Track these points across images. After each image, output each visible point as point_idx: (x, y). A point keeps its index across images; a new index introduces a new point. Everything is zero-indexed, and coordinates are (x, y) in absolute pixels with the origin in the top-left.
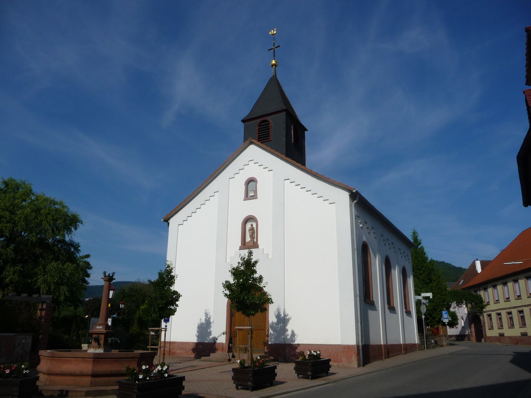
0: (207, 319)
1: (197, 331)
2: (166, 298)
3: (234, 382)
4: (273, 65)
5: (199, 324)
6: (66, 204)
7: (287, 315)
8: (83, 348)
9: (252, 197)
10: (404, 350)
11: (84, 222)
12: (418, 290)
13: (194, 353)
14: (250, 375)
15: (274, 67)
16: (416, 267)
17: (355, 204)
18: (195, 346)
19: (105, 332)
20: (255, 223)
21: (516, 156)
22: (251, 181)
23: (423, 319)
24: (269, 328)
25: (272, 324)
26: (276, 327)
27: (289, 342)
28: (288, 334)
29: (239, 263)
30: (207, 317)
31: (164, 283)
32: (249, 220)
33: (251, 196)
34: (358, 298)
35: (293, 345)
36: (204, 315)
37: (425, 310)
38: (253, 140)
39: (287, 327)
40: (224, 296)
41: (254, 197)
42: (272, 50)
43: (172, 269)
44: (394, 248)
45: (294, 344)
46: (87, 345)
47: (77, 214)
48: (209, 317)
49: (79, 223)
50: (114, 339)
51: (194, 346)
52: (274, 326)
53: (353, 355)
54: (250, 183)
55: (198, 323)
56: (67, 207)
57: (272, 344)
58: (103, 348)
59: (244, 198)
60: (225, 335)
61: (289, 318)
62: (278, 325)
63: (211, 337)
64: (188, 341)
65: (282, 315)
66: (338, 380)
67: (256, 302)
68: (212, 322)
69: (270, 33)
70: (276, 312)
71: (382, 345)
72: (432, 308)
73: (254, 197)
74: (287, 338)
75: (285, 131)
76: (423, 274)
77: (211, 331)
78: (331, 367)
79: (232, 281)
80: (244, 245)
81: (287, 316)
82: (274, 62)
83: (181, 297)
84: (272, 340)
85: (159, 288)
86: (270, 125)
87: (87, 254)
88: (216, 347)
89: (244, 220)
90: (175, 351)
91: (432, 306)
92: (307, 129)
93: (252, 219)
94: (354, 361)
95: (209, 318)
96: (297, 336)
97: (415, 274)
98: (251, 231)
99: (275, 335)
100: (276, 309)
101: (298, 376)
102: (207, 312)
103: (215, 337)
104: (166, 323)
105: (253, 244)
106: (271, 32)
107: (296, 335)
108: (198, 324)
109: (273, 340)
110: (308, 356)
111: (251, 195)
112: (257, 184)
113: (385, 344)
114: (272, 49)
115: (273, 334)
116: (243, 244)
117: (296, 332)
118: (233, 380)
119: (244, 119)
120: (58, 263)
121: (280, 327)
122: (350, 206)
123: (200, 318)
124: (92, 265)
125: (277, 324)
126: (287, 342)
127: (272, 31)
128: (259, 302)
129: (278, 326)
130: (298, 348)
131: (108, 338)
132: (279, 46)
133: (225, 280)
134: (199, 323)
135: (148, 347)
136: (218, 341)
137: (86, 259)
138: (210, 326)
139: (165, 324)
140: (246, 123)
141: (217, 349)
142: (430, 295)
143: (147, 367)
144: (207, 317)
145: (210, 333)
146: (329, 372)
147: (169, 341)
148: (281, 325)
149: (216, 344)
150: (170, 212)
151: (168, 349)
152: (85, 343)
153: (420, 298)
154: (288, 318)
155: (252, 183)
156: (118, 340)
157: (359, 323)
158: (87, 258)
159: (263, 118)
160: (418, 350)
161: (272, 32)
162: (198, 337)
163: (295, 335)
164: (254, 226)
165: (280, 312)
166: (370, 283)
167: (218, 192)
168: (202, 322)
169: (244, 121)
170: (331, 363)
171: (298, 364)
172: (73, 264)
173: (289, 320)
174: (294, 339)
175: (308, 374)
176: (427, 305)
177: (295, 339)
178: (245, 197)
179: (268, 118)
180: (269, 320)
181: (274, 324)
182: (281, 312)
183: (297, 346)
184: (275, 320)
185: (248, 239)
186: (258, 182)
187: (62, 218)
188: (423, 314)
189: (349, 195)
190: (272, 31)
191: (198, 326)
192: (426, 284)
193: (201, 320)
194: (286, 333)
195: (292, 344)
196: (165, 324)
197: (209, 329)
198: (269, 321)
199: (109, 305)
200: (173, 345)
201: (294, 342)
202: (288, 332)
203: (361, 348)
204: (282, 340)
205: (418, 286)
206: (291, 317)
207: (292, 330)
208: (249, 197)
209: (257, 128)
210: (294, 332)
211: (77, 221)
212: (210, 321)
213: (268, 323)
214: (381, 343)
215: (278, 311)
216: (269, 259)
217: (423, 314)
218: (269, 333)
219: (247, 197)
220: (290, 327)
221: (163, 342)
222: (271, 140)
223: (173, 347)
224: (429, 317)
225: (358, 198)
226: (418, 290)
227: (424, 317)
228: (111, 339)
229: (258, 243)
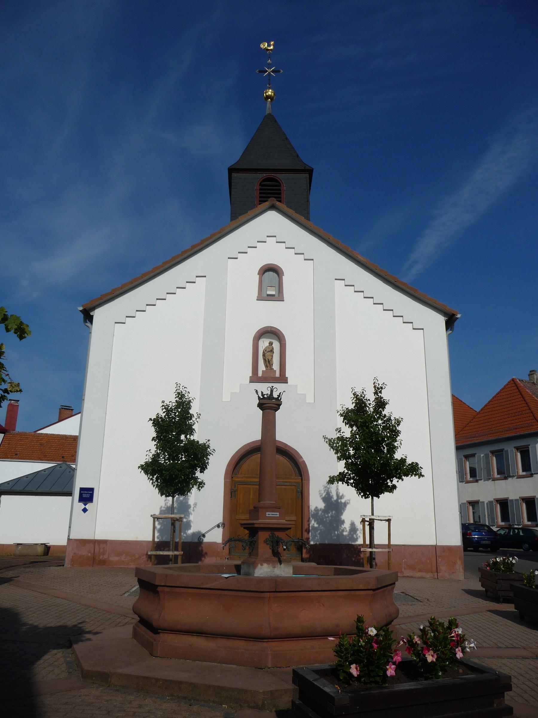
5: (163, 509)
7: (341, 496)
9: (270, 298)
24: (309, 518)
25: (315, 512)
26: (324, 517)
27: (346, 542)
28: (345, 528)
32: (262, 337)
33: (268, 295)
35: (355, 547)
39: (343, 517)
41: (279, 297)
45: (356, 545)
54: (271, 273)
55: (160, 507)
57: (316, 544)
60: (221, 530)
62: (328, 513)
63: (190, 532)
65: (335, 498)
68: (192, 506)
70: (323, 492)
73: (279, 297)
74: (344, 535)
77: (190, 521)
84: (316, 538)
88: (202, 550)
90: (106, 557)
99: (321, 530)
100: (323, 487)
103: (199, 533)
104: (85, 505)
110: (315, 543)
111: (269, 293)
115: (315, 529)
121: (331, 516)
125: (326, 510)
126: (343, 542)
136: (206, 540)
138: (188, 512)
139: (83, 506)
141: (206, 553)
145: (188, 525)
149: (202, 545)
151: (89, 554)
154: (343, 501)
166: (74, 483)
173: (345, 504)
174: (355, 536)
177: (356, 536)
180: (310, 504)
181: (320, 512)
182: (332, 492)
184: (321, 505)
185: (262, 367)
194: (341, 526)
195: (352, 545)
196: (83, 506)
197: (186, 519)
198: (309, 507)
199: (467, 525)
200: (102, 546)
201: (355, 542)
202: (345, 524)
204: (335, 538)
206: (349, 500)
210: (355, 525)
212: (188, 502)
213: (309, 509)
218: (310, 525)
219: (262, 297)
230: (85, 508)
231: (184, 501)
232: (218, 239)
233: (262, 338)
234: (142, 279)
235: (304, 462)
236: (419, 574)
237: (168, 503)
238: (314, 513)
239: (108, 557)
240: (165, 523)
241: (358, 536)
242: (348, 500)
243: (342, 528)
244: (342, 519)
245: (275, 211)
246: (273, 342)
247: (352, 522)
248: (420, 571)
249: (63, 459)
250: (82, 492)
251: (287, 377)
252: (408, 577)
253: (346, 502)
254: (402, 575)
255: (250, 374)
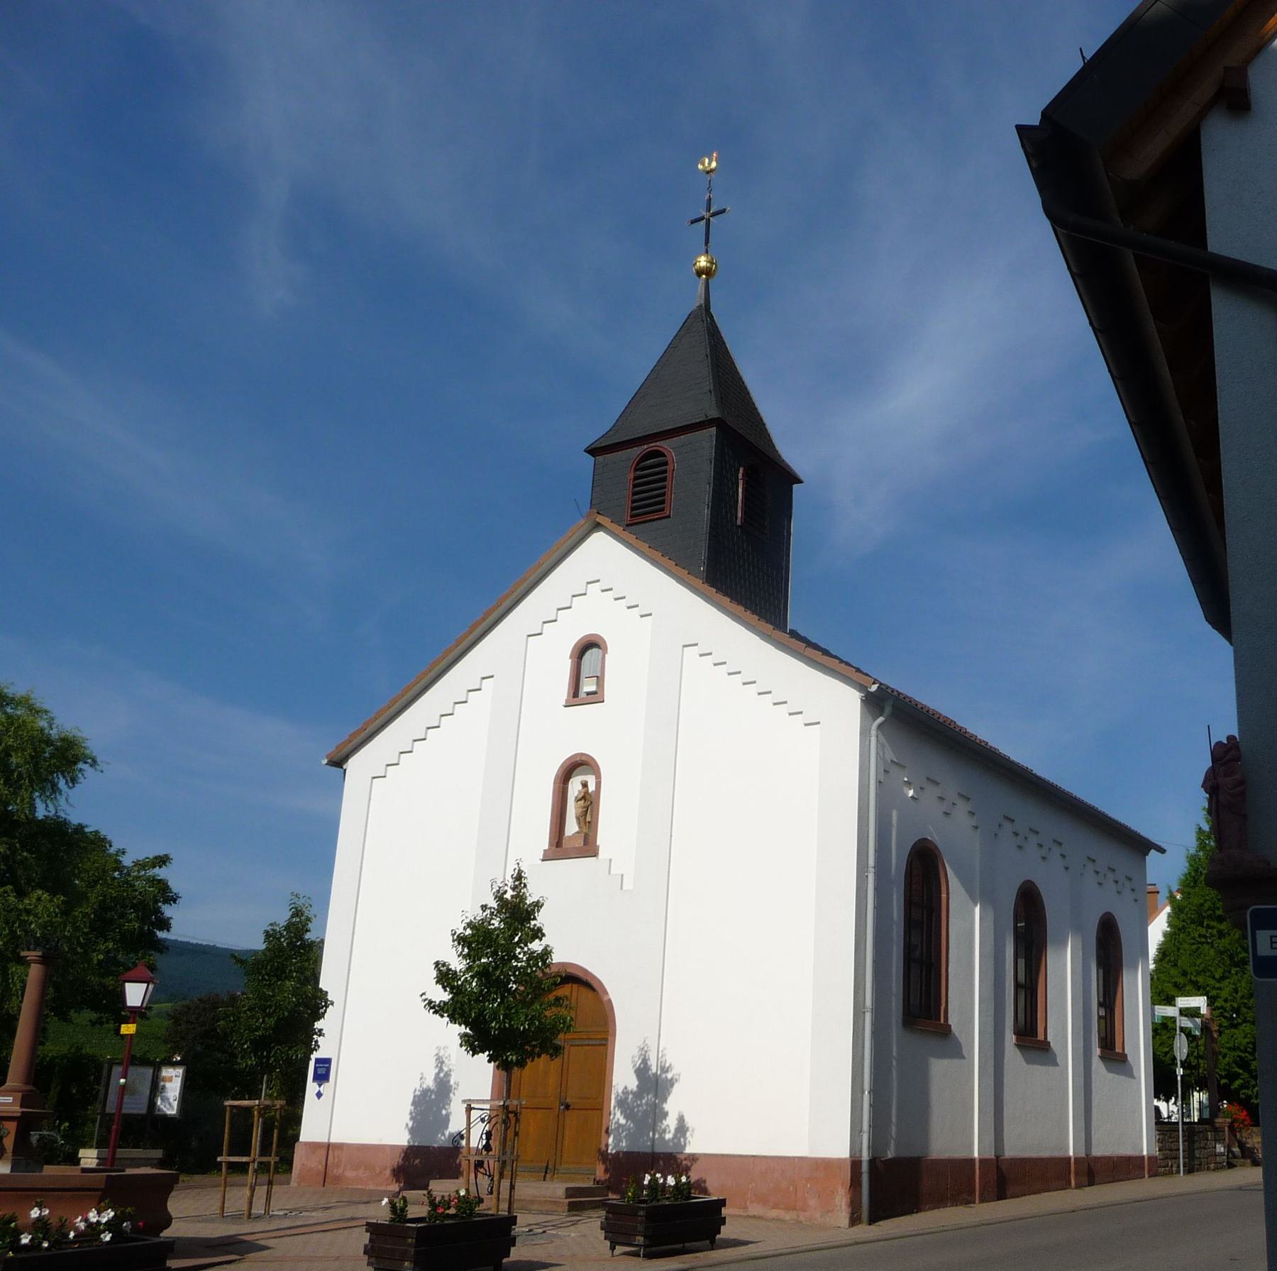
0: (442, 1075)
1: (411, 1113)
2: (274, 1012)
3: (368, 1263)
4: (699, 273)
5: (418, 1093)
6: (40, 701)
7: (668, 1068)
8: (82, 1161)
10: (1077, 1174)
11: (102, 762)
12: (1208, 985)
13: (397, 1181)
14: (410, 1240)
15: (704, 276)
16: (1208, 910)
17: (880, 727)
18: (403, 1160)
19: (19, 1115)
20: (594, 777)
21: (1204, 619)
22: (589, 646)
23: (1179, 1078)
28: (668, 1126)
29: (484, 907)
30: (441, 1070)
31: (276, 964)
32: (576, 771)
33: (588, 694)
34: (868, 1017)
36: (433, 1062)
37: (1185, 1051)
38: (600, 519)
40: (425, 1007)
41: (596, 697)
42: (703, 223)
43: (308, 919)
44: (1063, 856)
46: (97, 1150)
47: (80, 734)
48: (445, 1069)
49: (86, 763)
50: (48, 1133)
51: (400, 1160)
52: (630, 1100)
53: (840, 1189)
56: (46, 712)
58: (10, 1161)
59: (565, 698)
61: (672, 1079)
64: (381, 1140)
66: (714, 1265)
67: (517, 1028)
69: (700, 167)
71: (973, 1160)
72: (1248, 1043)
73: (596, 697)
75: (711, 488)
76: (1229, 935)
78: (724, 1224)
79: (457, 964)
80: (557, 847)
81: (667, 1071)
82: (703, 262)
83: (330, 1006)
85: (264, 979)
86: (669, 468)
87: (161, 854)
89: (562, 766)
91: (1249, 1036)
92: (801, 476)
93: (584, 765)
94: (839, 1208)
95: (448, 1075)
96: (693, 1131)
97: (1207, 931)
98: (583, 801)
99: (629, 1129)
101: (611, 1249)
102: (441, 1054)
104: (320, 1086)
105: (584, 844)
106: (704, 165)
107: (690, 1129)
108: (415, 1090)
109: (624, 1144)
112: (606, 655)
113: (990, 1154)
114: (702, 218)
116: (555, 844)
117: (689, 1122)
118: (367, 1257)
119: (593, 446)
120: (5, 892)
121: (647, 1104)
122: (860, 734)
123: (422, 1074)
124: (175, 890)
125: (639, 1094)
127: (707, 160)
128: (529, 1027)
129: (639, 1102)
130: (692, 1168)
131: (32, 1133)
132: (723, 211)
133: (435, 961)
134: (418, 1088)
135: (219, 1159)
137: (157, 870)
140: (600, 458)
142: (1200, 1002)
143: (43, 1214)
144: (441, 1070)
146: (718, 1236)
147: (326, 1141)
148: (648, 1099)
150: (348, 738)
151: (320, 1166)
152: (91, 1147)
153: (1170, 1011)
154: (669, 1076)
155: (595, 650)
156: (59, 1137)
157: (866, 1092)
158: (160, 867)
159: (651, 445)
160: (1147, 1176)
161: (706, 165)
162: (412, 1131)
163: (688, 1128)
164: (592, 788)
165: (647, 1058)
167: (492, 677)
168: (425, 1086)
169: (593, 451)
170: (724, 1211)
171: (612, 1213)
172: (54, 896)
173: (671, 1083)
175: (636, 1243)
176: (1197, 1033)
177: (685, 1141)
178: (568, 696)
179: (664, 445)
181: (631, 1096)
183: (689, 1164)
184: (633, 1084)
185: (572, 827)
186: (609, 651)
187: (24, 750)
188: (1179, 1062)
189: (860, 700)
190: (707, 160)
191: (415, 1097)
192: (1235, 967)
193: (423, 1080)
194: (661, 1122)
197: (446, 1109)
202: (668, 1119)
203: (865, 1167)
205: (1211, 971)
206: (679, 1075)
207: (679, 1113)
208: (582, 695)
209: (632, 476)
210: (684, 1121)
211: (79, 760)
214: (1069, 1153)
215: (641, 1055)
216: (625, 891)
217: (1179, 1062)
219: (575, 695)
220: (674, 1106)
221: (473, 1148)
222: (669, 517)
223: (336, 1160)
224: (1236, 1069)
225: (888, 710)
226: (1208, 985)
227: (1182, 1073)
228: (40, 1135)
229: (596, 842)
230: (319, 1091)
231: (444, 1080)
232: (379, 728)
233: (577, 775)
234: (484, 623)
235: (610, 1001)
236: (774, 1213)
237: (424, 1083)
238: (621, 1098)
239: (343, 1172)
240: (419, 1118)
241: (687, 1141)
242: (677, 1074)
243: (663, 1127)
244: (666, 1110)
245: (604, 532)
246: (586, 779)
247: (681, 1114)
248: (775, 1206)
249: (1159, 1121)
250: (317, 1065)
251: (598, 847)
252: (754, 1217)
253: (675, 1077)
254: (746, 1214)
255: (545, 844)
